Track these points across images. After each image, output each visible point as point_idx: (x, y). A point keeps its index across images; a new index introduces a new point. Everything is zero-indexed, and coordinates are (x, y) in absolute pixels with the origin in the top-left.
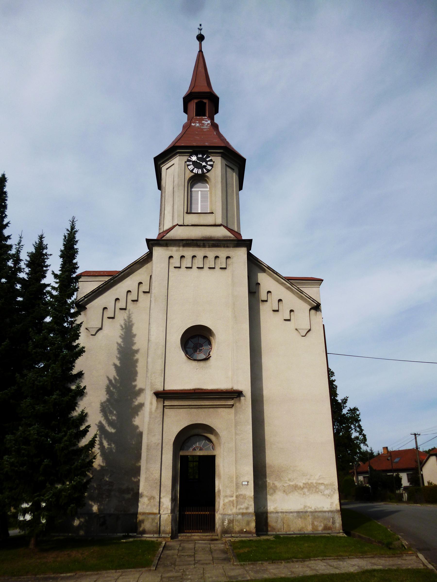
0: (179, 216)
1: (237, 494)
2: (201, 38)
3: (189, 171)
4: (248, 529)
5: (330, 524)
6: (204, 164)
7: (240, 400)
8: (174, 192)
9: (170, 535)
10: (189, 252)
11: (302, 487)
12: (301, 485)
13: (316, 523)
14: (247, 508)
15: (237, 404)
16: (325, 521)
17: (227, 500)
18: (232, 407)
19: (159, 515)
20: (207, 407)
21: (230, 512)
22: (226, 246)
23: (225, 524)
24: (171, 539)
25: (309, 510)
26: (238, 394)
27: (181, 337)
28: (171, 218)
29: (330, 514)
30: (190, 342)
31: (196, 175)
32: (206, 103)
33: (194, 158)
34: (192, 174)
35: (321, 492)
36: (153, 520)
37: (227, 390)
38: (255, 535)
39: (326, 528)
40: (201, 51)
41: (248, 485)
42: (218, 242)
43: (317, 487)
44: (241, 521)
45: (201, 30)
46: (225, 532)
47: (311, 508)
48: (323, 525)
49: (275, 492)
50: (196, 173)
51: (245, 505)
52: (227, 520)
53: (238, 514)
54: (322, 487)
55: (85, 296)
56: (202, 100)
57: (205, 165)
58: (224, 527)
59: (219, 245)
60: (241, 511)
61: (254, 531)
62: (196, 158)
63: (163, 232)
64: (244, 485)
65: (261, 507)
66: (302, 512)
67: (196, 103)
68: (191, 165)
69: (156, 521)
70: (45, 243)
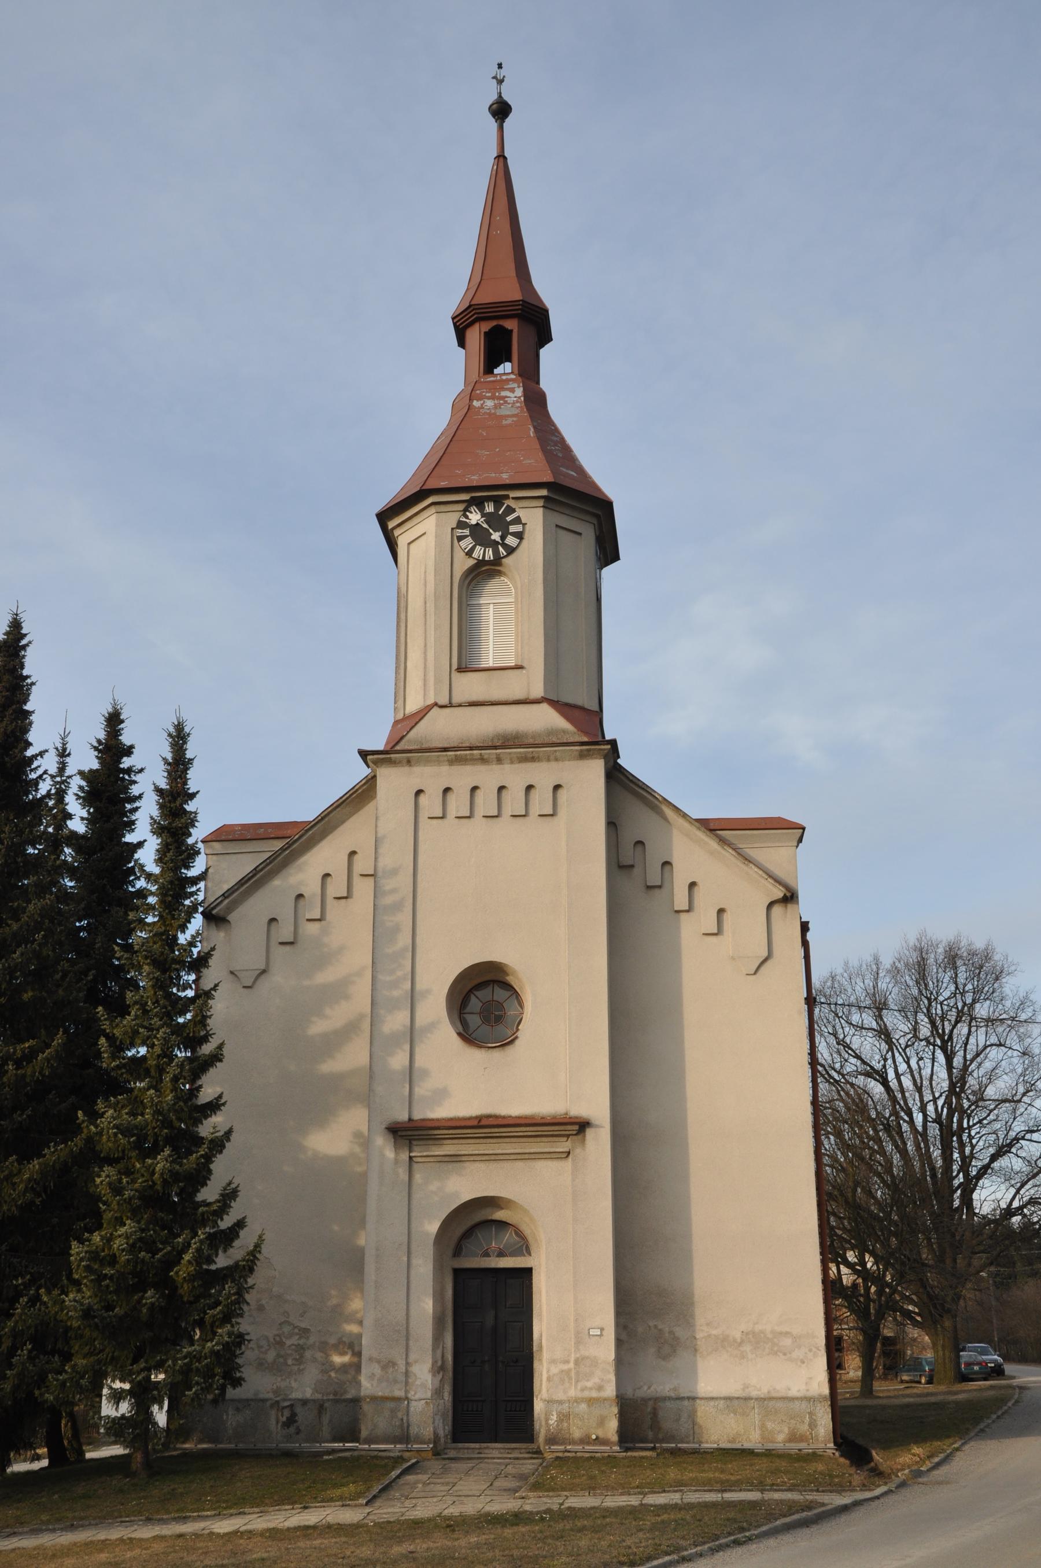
0: (438, 681)
1: (578, 1356)
2: (501, 111)
3: (463, 554)
4: (601, 1434)
5: (804, 1428)
6: (496, 536)
7: (583, 1141)
8: (425, 615)
9: (431, 1446)
10: (462, 777)
11: (739, 1340)
12: (738, 1336)
13: (770, 1425)
14: (600, 1388)
15: (578, 1151)
16: (792, 1421)
17: (554, 1370)
18: (567, 1157)
19: (406, 1402)
20: (507, 1157)
21: (560, 1396)
22: (552, 757)
23: (551, 1422)
24: (434, 1455)
25: (754, 1393)
26: (582, 1126)
27: (446, 991)
28: (421, 683)
29: (804, 1404)
30: (473, 998)
31: (481, 563)
32: (511, 331)
33: (475, 517)
34: (471, 562)
35: (785, 1354)
36: (393, 1411)
37: (554, 1117)
38: (617, 1448)
39: (793, 1437)
40: (501, 158)
41: (601, 1335)
42: (531, 750)
43: (775, 1340)
44: (586, 1416)
45: (500, 82)
46: (552, 1440)
47: (759, 1390)
48: (786, 1430)
49: (675, 1351)
50: (481, 558)
51: (595, 1380)
52: (554, 1413)
53: (577, 1401)
54: (787, 1342)
55: (223, 895)
56: (502, 322)
57: (498, 539)
58: (549, 1430)
59: (536, 755)
60: (586, 1394)
61: (615, 1438)
62: (479, 516)
63: (406, 718)
64: (593, 1335)
65: (642, 1387)
66: (738, 1398)
67: (485, 333)
68: (466, 536)
69: (400, 1415)
70: (126, 739)
